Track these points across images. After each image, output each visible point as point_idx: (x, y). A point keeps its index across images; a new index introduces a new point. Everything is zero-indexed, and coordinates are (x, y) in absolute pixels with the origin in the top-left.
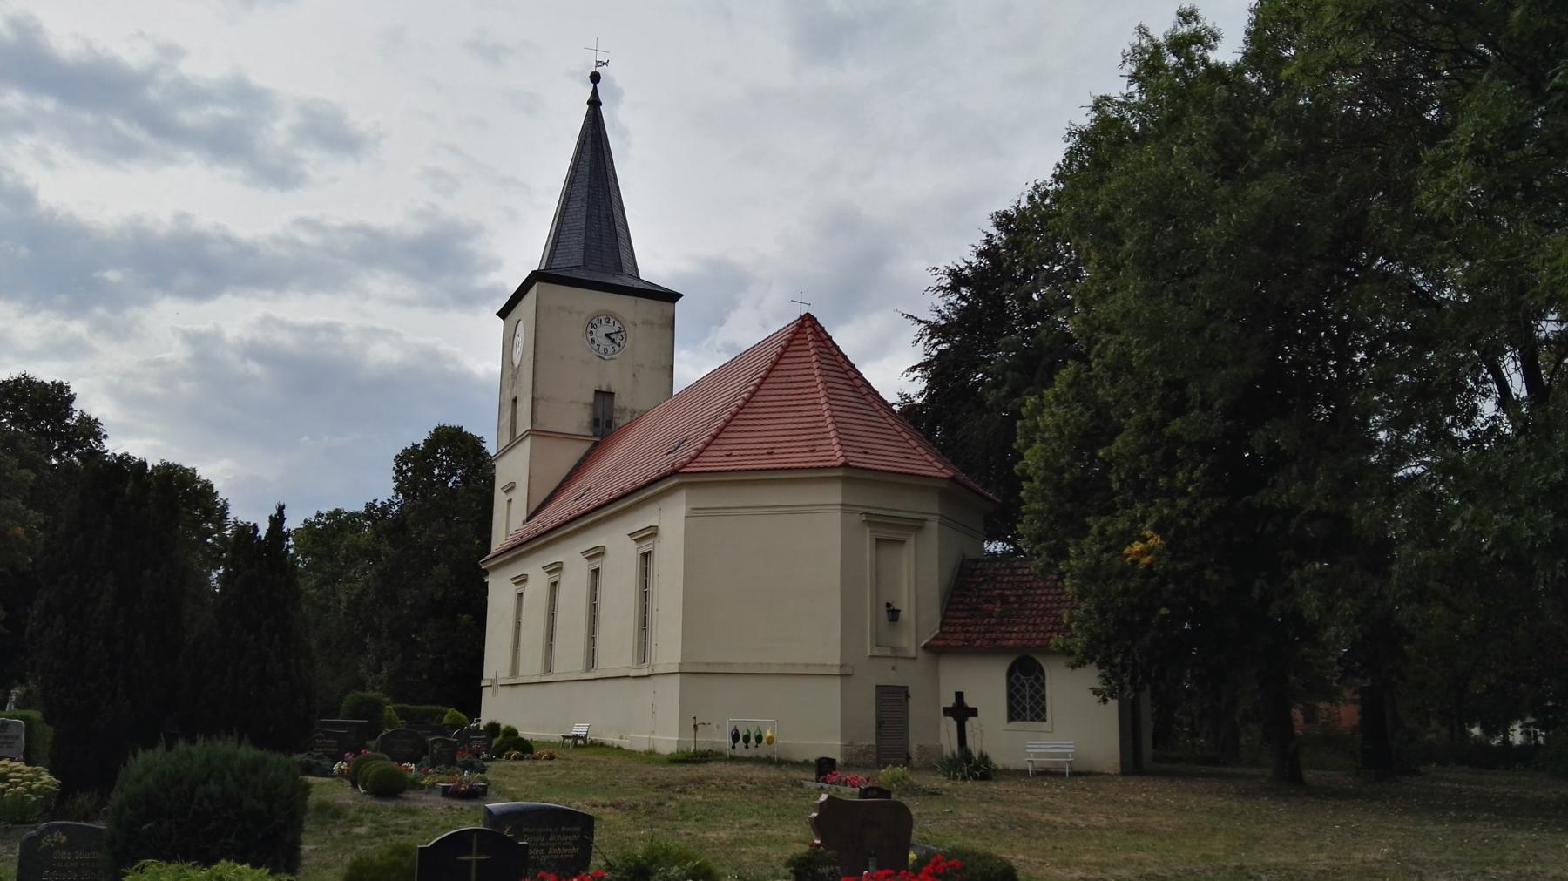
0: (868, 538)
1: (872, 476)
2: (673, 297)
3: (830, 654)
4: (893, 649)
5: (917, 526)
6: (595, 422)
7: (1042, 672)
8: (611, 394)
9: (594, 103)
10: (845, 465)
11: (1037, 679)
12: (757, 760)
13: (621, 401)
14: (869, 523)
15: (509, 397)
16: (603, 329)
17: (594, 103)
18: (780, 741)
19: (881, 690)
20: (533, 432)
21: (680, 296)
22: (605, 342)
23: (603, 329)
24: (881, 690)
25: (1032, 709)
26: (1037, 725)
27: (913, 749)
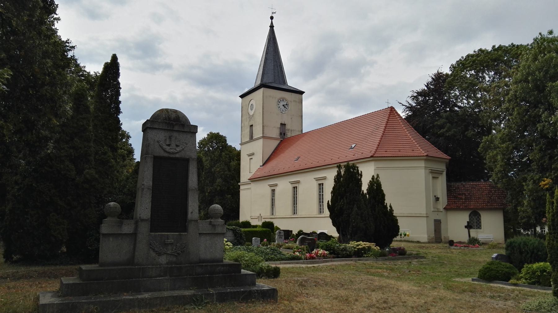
0: (431, 176)
1: (432, 158)
2: (302, 93)
3: (423, 212)
4: (438, 209)
5: (440, 173)
6: (281, 134)
7: (480, 215)
8: (285, 125)
9: (272, 27)
10: (427, 156)
11: (478, 217)
12: (405, 241)
13: (288, 127)
14: (431, 172)
15: (247, 124)
16: (282, 103)
17: (272, 27)
18: (411, 235)
19: (435, 220)
20: (263, 137)
21: (304, 92)
22: (283, 107)
23: (282, 103)
24: (435, 220)
25: (477, 226)
26: (479, 230)
27: (443, 238)
